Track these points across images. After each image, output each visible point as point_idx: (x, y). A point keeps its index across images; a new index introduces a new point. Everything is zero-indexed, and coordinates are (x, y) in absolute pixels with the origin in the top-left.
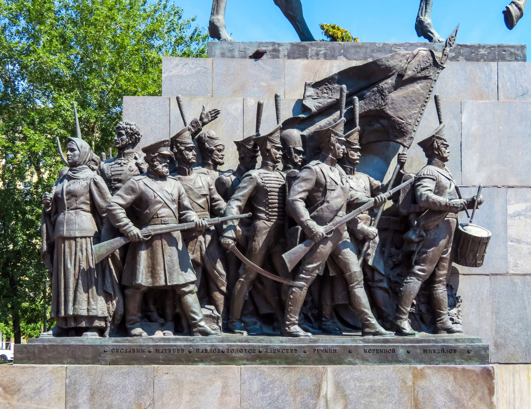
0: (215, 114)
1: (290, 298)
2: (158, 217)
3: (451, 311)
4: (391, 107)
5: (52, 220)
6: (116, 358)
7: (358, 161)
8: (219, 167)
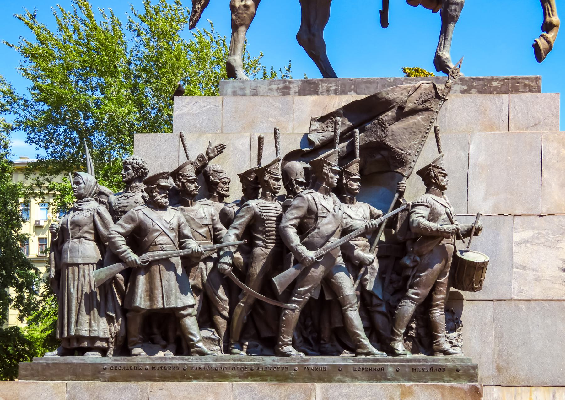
0: (221, 149)
1: (283, 320)
2: (156, 245)
3: (450, 335)
4: (391, 138)
5: (59, 249)
6: (115, 375)
7: (357, 191)
8: (226, 200)
